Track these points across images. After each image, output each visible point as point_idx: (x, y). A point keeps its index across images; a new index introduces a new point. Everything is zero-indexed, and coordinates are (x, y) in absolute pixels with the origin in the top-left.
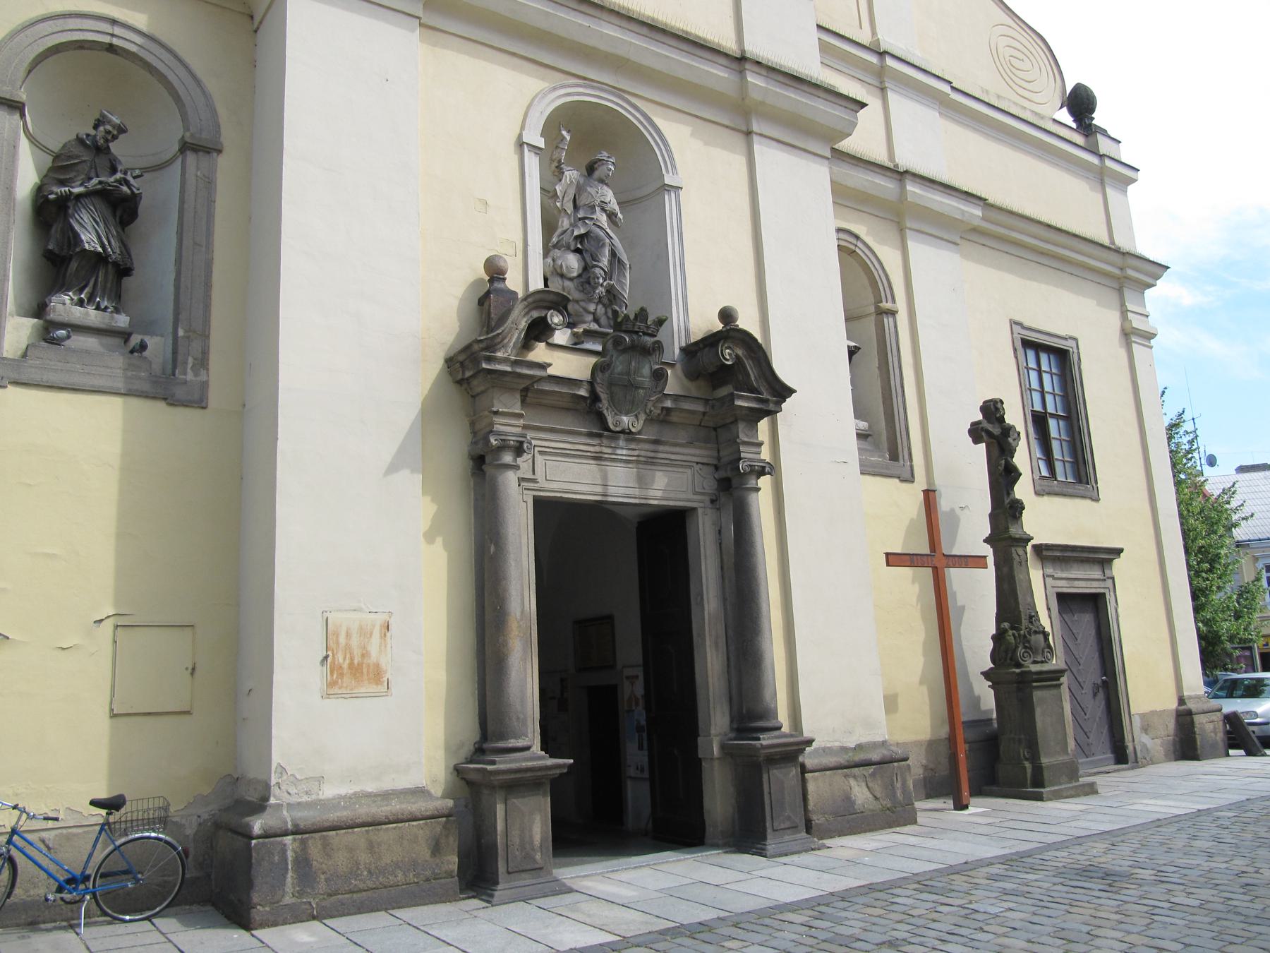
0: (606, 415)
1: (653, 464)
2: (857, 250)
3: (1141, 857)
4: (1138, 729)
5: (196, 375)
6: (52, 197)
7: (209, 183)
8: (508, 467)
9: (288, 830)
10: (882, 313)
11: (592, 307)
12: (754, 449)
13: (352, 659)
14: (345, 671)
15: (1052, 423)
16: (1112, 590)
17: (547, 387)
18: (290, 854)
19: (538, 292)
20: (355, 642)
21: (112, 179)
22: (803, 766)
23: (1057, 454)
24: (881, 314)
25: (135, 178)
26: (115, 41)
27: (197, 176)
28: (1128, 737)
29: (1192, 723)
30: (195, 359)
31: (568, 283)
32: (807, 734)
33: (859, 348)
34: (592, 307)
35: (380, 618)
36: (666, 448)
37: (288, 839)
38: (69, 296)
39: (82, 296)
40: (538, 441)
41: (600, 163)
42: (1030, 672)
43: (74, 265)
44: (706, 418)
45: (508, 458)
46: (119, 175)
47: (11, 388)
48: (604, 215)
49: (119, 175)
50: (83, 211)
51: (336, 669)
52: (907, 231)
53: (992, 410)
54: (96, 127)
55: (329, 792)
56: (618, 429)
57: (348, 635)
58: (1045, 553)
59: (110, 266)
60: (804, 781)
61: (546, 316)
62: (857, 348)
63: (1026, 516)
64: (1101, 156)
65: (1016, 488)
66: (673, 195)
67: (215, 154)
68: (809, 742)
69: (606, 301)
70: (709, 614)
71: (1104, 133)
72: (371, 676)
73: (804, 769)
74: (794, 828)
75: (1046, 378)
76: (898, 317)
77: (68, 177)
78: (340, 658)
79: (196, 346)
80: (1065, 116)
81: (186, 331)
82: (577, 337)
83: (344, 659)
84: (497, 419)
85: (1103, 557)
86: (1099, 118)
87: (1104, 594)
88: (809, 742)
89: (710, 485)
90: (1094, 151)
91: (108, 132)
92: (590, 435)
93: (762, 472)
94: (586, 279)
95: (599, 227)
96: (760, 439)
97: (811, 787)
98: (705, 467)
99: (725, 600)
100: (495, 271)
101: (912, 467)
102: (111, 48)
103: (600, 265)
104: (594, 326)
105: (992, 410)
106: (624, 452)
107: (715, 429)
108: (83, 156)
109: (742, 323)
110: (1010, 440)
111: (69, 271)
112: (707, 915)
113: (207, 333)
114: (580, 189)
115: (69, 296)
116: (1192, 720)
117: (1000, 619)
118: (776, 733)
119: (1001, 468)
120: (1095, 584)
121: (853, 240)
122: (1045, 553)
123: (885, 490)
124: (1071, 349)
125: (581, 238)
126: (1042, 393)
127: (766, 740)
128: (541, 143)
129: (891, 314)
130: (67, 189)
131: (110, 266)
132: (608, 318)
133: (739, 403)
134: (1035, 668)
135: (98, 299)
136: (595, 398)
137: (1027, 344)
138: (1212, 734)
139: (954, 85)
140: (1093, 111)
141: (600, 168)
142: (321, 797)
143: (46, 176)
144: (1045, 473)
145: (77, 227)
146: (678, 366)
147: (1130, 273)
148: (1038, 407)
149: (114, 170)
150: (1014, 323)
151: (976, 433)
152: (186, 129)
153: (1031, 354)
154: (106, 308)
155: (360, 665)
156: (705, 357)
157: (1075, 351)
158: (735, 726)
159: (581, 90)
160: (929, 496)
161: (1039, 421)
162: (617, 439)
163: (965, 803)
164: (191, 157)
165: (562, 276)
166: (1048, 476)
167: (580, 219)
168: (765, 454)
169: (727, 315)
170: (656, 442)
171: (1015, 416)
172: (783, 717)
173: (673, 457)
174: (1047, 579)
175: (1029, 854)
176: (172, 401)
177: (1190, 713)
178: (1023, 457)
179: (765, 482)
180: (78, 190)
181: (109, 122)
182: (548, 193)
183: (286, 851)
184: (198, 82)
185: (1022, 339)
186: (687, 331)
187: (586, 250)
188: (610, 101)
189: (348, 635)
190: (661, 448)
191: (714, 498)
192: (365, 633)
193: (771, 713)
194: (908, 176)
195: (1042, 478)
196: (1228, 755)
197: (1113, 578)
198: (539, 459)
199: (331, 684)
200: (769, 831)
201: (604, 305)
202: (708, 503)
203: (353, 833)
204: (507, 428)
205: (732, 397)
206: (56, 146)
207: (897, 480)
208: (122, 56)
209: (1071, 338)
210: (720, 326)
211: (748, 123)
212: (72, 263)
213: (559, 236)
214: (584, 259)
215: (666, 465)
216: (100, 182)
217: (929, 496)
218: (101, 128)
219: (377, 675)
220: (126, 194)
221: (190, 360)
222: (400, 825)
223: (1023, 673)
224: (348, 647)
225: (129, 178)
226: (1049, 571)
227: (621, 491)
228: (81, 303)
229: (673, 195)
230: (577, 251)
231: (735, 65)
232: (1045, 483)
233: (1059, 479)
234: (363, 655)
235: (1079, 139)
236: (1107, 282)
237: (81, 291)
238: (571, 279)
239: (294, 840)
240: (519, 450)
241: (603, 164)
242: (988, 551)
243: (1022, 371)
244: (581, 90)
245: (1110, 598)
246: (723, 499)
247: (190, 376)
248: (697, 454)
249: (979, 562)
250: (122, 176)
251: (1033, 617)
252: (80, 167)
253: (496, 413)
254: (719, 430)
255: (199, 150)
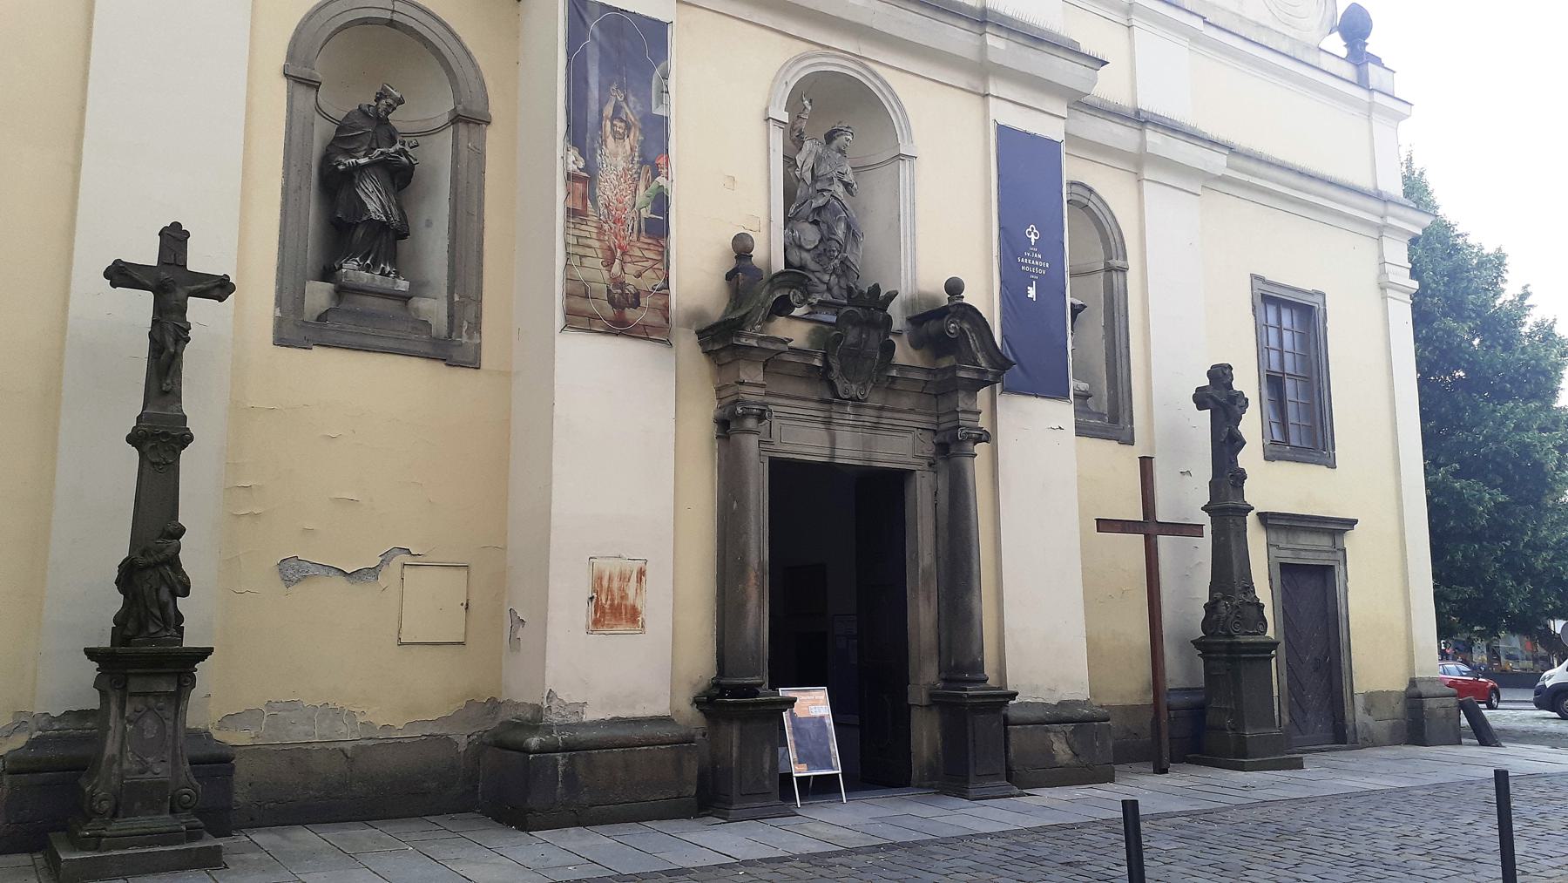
0: (837, 383)
1: (877, 428)
2: (1090, 205)
3: (1317, 820)
4: (1361, 709)
5: (470, 338)
6: (341, 167)
7: (480, 155)
8: (750, 432)
9: (559, 747)
10: (1109, 269)
11: (826, 278)
12: (973, 417)
13: (613, 600)
14: (607, 611)
15: (1289, 385)
16: (1342, 562)
17: (786, 357)
18: (560, 769)
19: (781, 273)
20: (615, 585)
21: (392, 150)
22: (1006, 718)
23: (1292, 417)
24: (1110, 271)
25: (411, 148)
26: (396, 17)
27: (468, 147)
28: (1348, 716)
29: (1422, 706)
30: (469, 323)
31: (805, 255)
32: (1011, 688)
33: (1083, 307)
34: (826, 278)
35: (636, 566)
36: (889, 414)
37: (559, 756)
38: (356, 261)
39: (368, 262)
40: (778, 407)
41: (839, 133)
42: (1239, 643)
43: (360, 232)
44: (929, 386)
45: (751, 423)
46: (398, 146)
47: (315, 349)
48: (842, 186)
49: (398, 146)
50: (368, 181)
51: (598, 607)
52: (1145, 182)
53: (1221, 375)
54: (378, 100)
55: (590, 715)
56: (846, 397)
57: (610, 579)
58: (1269, 522)
59: (391, 234)
60: (1006, 733)
61: (788, 296)
62: (1083, 307)
63: (1247, 485)
64: (1371, 90)
65: (1239, 457)
66: (907, 163)
67: (484, 126)
68: (1013, 695)
69: (839, 272)
70: (923, 571)
71: (1378, 61)
72: (629, 616)
73: (1007, 721)
74: (995, 776)
75: (1287, 336)
76: (1129, 274)
77: (352, 147)
78: (603, 598)
79: (470, 311)
80: (1336, 44)
81: (460, 297)
82: (811, 307)
83: (606, 601)
84: (744, 389)
85: (1337, 528)
86: (1373, 45)
87: (1332, 567)
88: (1013, 695)
89: (928, 449)
90: (1362, 82)
91: (390, 105)
92: (822, 401)
93: (978, 440)
94: (823, 251)
95: (836, 198)
96: (979, 408)
97: (1013, 738)
98: (925, 432)
99: (937, 558)
100: (742, 248)
101: (1132, 429)
102: (391, 23)
103: (836, 237)
104: (828, 297)
105: (1221, 375)
106: (852, 417)
107: (936, 396)
108: (365, 127)
109: (970, 297)
110: (1237, 408)
111: (355, 237)
112: (914, 837)
113: (479, 299)
114: (819, 159)
115: (356, 261)
116: (1422, 703)
117: (1213, 588)
118: (982, 686)
119: (1224, 436)
120: (1324, 556)
121: (1087, 194)
122: (1269, 522)
123: (1104, 450)
124: (1317, 306)
125: (818, 210)
126: (1281, 353)
127: (972, 690)
128: (785, 117)
129: (1122, 271)
130: (354, 160)
131: (391, 234)
132: (840, 287)
133: (962, 374)
134: (1243, 639)
135: (382, 265)
136: (827, 367)
137: (1267, 299)
138: (1444, 720)
139: (1208, 20)
140: (1367, 35)
141: (839, 138)
142: (584, 720)
143: (331, 144)
144: (1277, 437)
145: (363, 196)
146: (905, 335)
147: (1390, 221)
148: (1275, 367)
149: (393, 143)
150: (1255, 278)
151: (1201, 399)
152: (458, 102)
153: (1272, 311)
154: (390, 273)
155: (620, 605)
156: (932, 327)
157: (1322, 308)
158: (944, 675)
159: (824, 60)
160: (1146, 464)
161: (1274, 383)
162: (847, 405)
163: (1165, 766)
164: (462, 127)
165: (800, 247)
166: (1281, 440)
167: (818, 191)
168: (983, 422)
169: (954, 287)
170: (882, 408)
171: (1246, 382)
172: (989, 669)
173: (895, 422)
174: (1271, 549)
175: (1217, 811)
176: (451, 363)
177: (1420, 696)
178: (1251, 425)
179: (981, 449)
180: (362, 161)
181: (391, 95)
182: (789, 161)
183: (557, 765)
184: (468, 54)
185: (1262, 295)
186: (914, 280)
187: (824, 222)
188: (852, 70)
189: (610, 579)
190: (885, 414)
191: (932, 461)
192: (624, 578)
193: (979, 667)
194: (1149, 126)
195: (1273, 442)
196: (1460, 743)
197: (1344, 550)
198: (776, 422)
199: (596, 622)
200: (972, 775)
201: (837, 275)
202: (926, 466)
203: (612, 752)
204: (752, 395)
205: (954, 369)
206: (341, 116)
207: (1116, 443)
208: (400, 30)
209: (1318, 293)
210: (945, 299)
211: (986, 86)
212: (358, 229)
213: (797, 208)
214: (820, 229)
215: (889, 430)
216: (382, 153)
217: (1146, 464)
218: (383, 102)
219: (633, 615)
220: (405, 164)
221: (465, 324)
222: (651, 748)
223: (1232, 643)
224: (609, 589)
225: (407, 149)
226: (1273, 537)
227: (847, 454)
228: (368, 269)
229: (907, 163)
230: (815, 223)
231: (976, 29)
232: (1276, 448)
233: (1292, 443)
234: (622, 598)
235: (1348, 71)
236: (1365, 231)
237: (364, 259)
238: (808, 251)
239: (564, 757)
240: (761, 417)
241: (842, 134)
242: (1205, 520)
243: (1261, 329)
244: (824, 60)
245: (1339, 570)
246: (940, 463)
247: (465, 339)
248: (919, 420)
249: (1195, 530)
250: (401, 147)
251: (1249, 588)
252: (361, 138)
253: (742, 383)
254: (939, 397)
255: (470, 122)
